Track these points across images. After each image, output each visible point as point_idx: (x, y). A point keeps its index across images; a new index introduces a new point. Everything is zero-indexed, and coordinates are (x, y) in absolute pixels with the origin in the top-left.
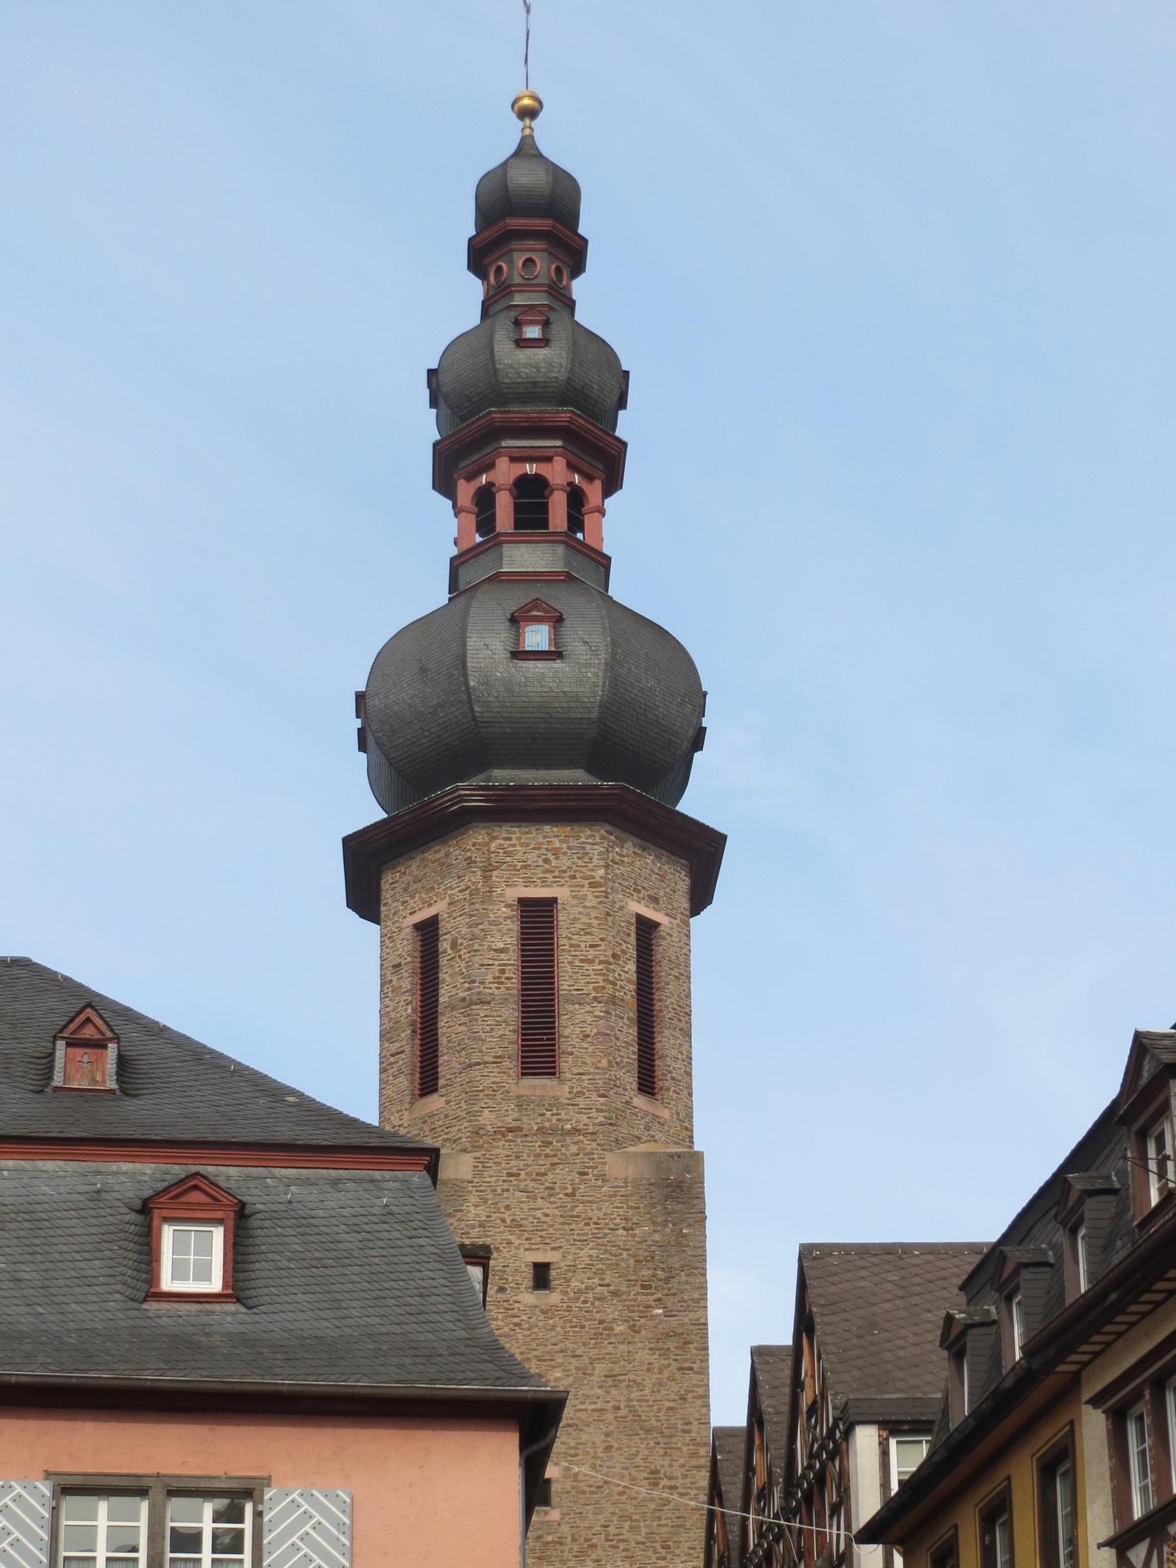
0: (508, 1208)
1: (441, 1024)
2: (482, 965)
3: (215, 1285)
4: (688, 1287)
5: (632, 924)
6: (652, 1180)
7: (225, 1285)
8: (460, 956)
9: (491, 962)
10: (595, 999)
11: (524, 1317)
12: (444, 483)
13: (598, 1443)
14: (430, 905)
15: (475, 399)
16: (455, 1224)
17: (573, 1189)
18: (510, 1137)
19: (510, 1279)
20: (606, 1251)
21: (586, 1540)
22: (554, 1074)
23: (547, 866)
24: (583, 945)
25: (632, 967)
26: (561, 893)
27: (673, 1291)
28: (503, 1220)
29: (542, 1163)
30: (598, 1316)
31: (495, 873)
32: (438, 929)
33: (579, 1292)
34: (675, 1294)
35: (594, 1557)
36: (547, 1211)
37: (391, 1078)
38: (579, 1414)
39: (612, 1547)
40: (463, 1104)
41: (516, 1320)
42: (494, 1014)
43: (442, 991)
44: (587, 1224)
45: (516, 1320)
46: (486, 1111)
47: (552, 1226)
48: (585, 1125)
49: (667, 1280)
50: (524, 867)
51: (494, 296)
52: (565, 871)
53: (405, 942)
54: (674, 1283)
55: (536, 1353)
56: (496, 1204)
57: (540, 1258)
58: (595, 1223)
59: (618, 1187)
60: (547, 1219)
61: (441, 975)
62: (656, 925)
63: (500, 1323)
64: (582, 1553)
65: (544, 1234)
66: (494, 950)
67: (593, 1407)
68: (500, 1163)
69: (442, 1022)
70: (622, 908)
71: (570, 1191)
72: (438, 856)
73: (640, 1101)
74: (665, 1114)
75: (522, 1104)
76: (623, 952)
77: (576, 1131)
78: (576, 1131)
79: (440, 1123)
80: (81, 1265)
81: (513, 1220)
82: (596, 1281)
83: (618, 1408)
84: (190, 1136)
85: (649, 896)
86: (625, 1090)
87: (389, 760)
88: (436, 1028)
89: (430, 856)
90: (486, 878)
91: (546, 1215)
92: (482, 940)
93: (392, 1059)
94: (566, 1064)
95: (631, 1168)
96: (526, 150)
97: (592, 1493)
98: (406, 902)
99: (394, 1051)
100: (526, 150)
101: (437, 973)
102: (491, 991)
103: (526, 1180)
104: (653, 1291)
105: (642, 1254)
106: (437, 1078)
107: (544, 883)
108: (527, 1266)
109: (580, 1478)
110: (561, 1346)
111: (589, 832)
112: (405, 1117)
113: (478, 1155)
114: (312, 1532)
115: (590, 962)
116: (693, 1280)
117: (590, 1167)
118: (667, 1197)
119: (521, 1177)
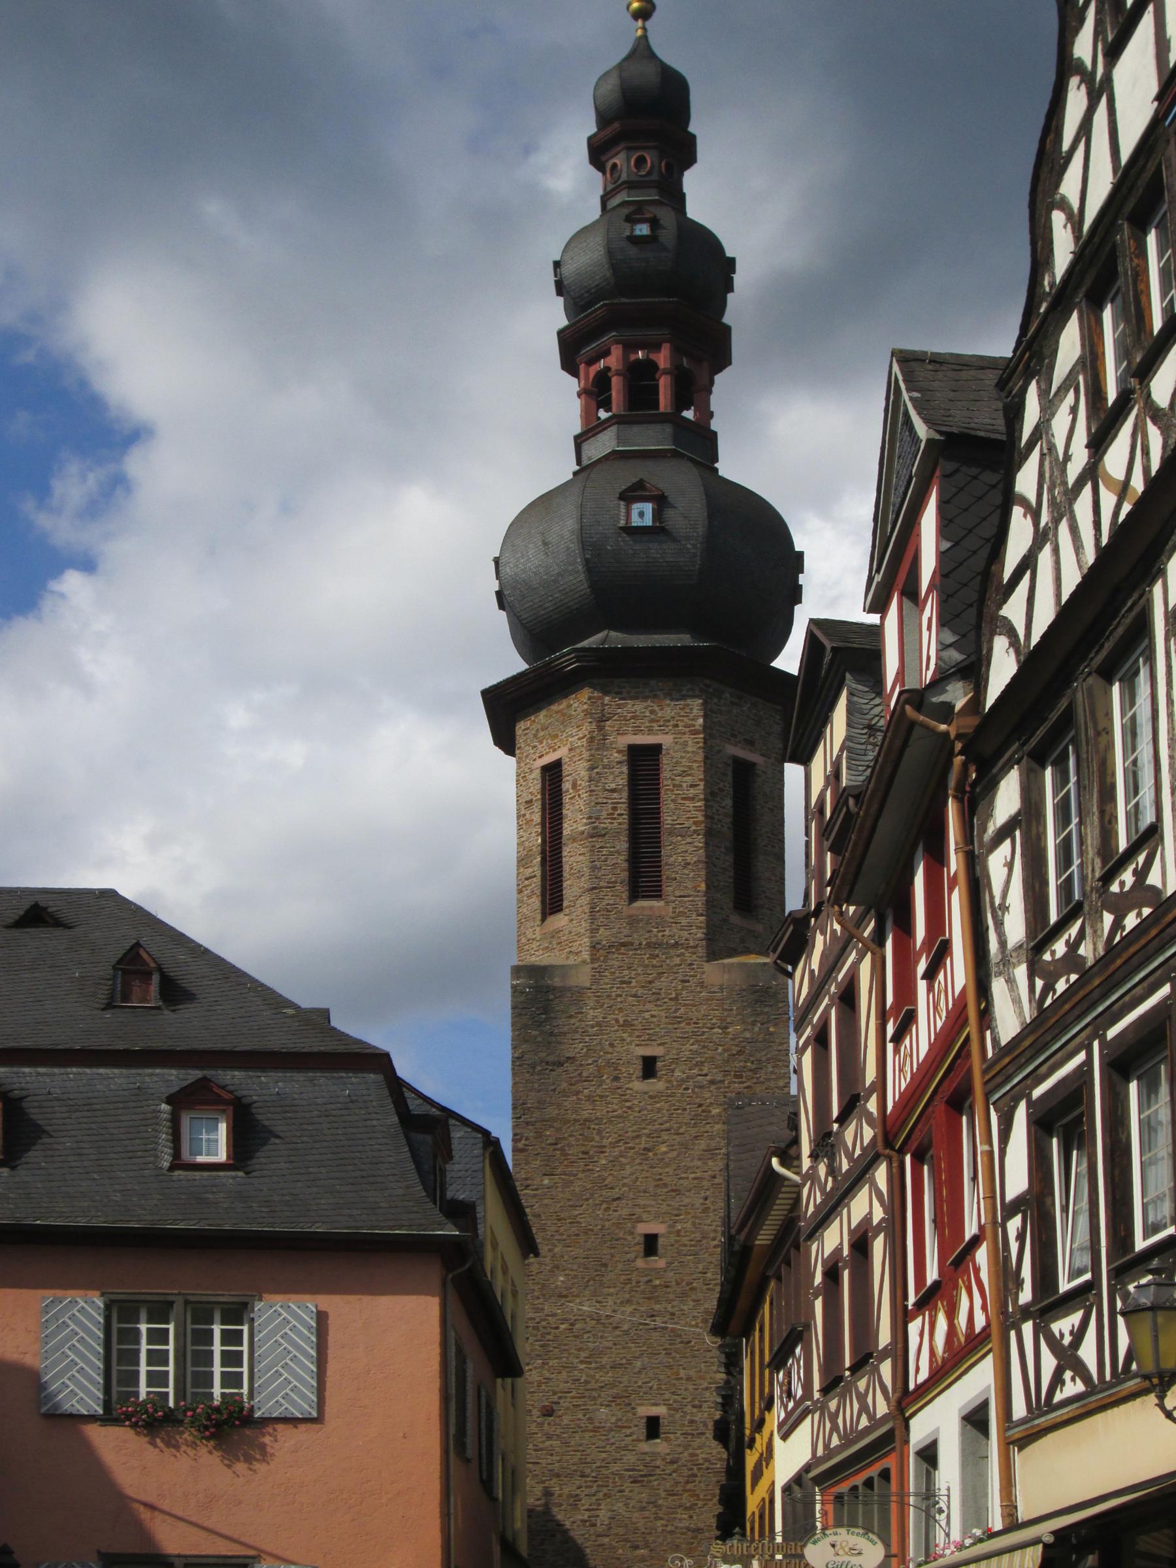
0: (621, 1010)
1: (564, 853)
2: (597, 803)
3: (222, 1156)
4: (773, 1076)
5: (729, 765)
6: (744, 987)
7: (228, 1157)
8: (579, 795)
9: (605, 801)
10: (695, 831)
11: (636, 1102)
12: (569, 364)
13: (697, 1205)
14: (555, 750)
15: (593, 291)
16: (577, 1024)
17: (677, 994)
18: (622, 951)
19: (624, 1070)
20: (704, 1047)
21: (688, 1284)
22: (660, 896)
23: (653, 717)
24: (684, 785)
25: (729, 802)
26: (665, 740)
27: (762, 1079)
28: (617, 1021)
29: (650, 972)
30: (698, 1100)
31: (608, 723)
32: (561, 771)
33: (683, 1081)
34: (763, 1083)
35: (694, 1297)
36: (654, 1013)
37: (525, 898)
38: (681, 1181)
39: (708, 1289)
40: (583, 923)
41: (628, 1104)
42: (608, 845)
43: (565, 825)
44: (689, 1024)
45: (628, 1104)
46: (602, 929)
47: (659, 1025)
48: (686, 940)
49: (754, 1071)
50: (632, 717)
51: (612, 190)
52: (669, 721)
53: (535, 782)
54: (762, 1075)
55: (645, 1131)
56: (611, 1007)
57: (648, 1052)
58: (694, 1023)
59: (714, 992)
60: (655, 1020)
61: (564, 812)
62: (753, 765)
63: (615, 1107)
64: (684, 1294)
65: (651, 1032)
66: (607, 790)
67: (693, 1176)
68: (614, 973)
69: (565, 851)
70: (719, 751)
71: (673, 996)
72: (561, 707)
73: (735, 919)
74: (759, 928)
75: (633, 921)
76: (722, 790)
77: (676, 945)
78: (676, 945)
79: (565, 938)
80: (126, 1142)
81: (625, 1021)
82: (695, 1071)
83: (714, 1177)
84: (209, 1046)
85: (745, 740)
86: (722, 909)
87: (520, 621)
88: (561, 857)
89: (555, 707)
90: (601, 728)
91: (653, 1016)
92: (598, 782)
93: (526, 882)
94: (668, 889)
95: (726, 976)
96: (642, 50)
97: (691, 1246)
98: (535, 747)
99: (528, 875)
100: (642, 50)
101: (561, 809)
102: (605, 826)
103: (635, 987)
104: (744, 1080)
105: (735, 1050)
106: (562, 900)
107: (650, 731)
108: (637, 1059)
109: (682, 1233)
110: (667, 1125)
111: (689, 686)
112: (537, 932)
113: (596, 965)
114: (289, 1332)
115: (692, 799)
116: (777, 1071)
117: (691, 976)
118: (757, 1001)
119: (632, 985)
